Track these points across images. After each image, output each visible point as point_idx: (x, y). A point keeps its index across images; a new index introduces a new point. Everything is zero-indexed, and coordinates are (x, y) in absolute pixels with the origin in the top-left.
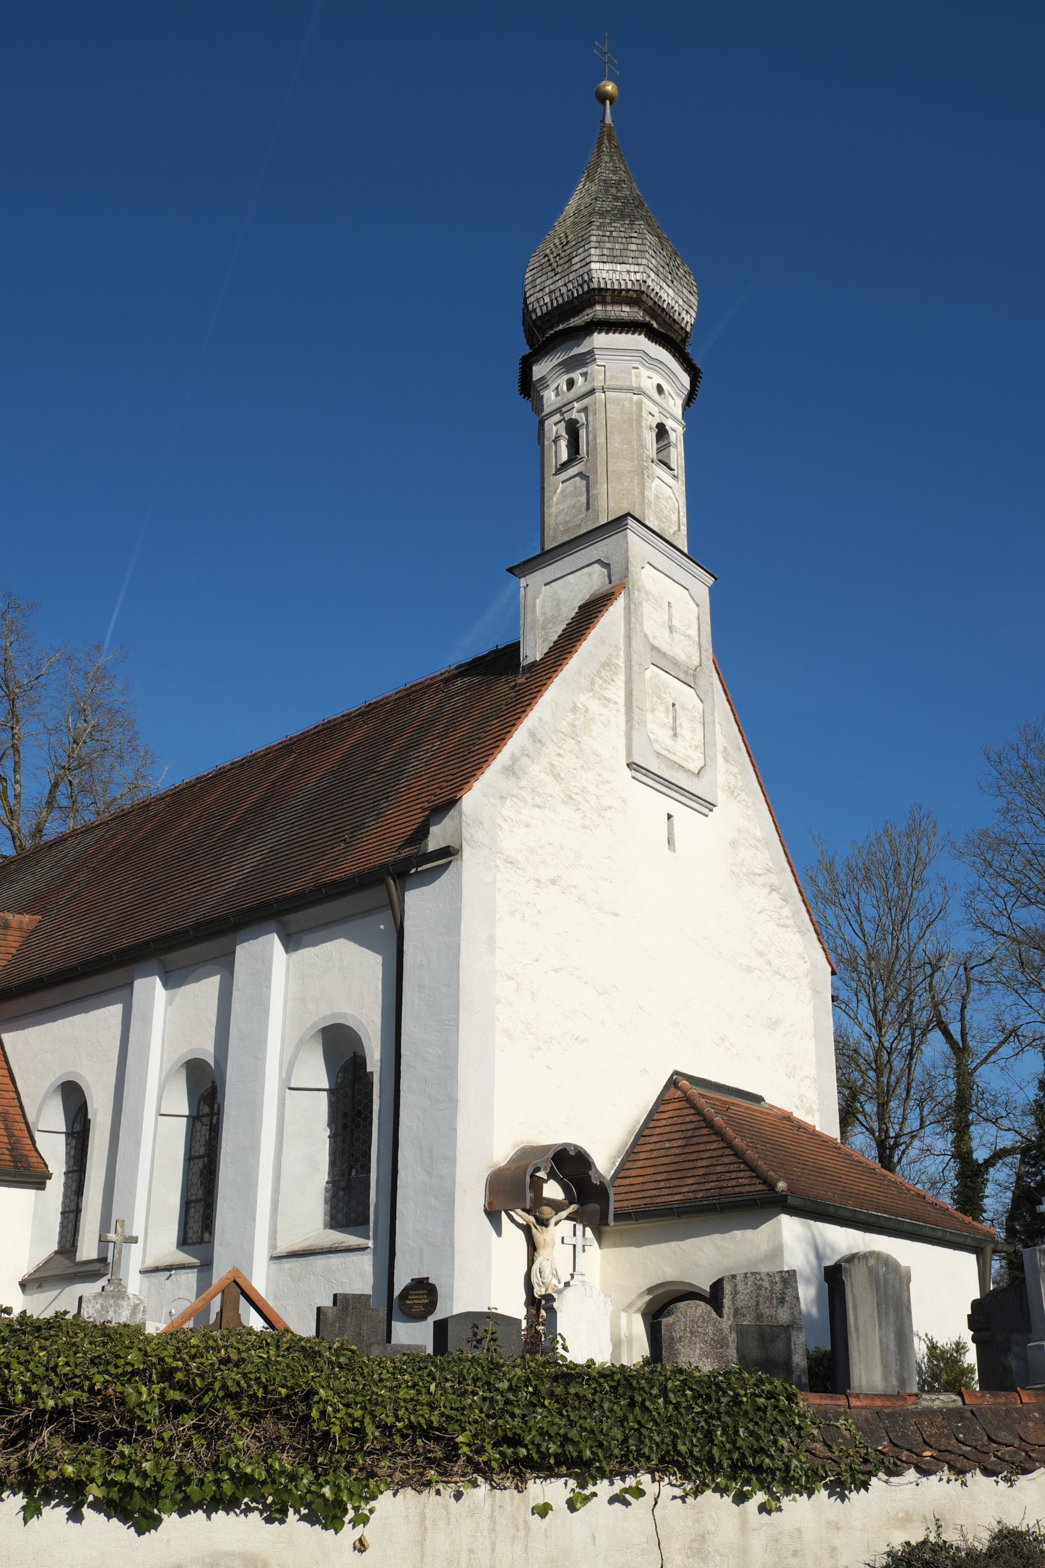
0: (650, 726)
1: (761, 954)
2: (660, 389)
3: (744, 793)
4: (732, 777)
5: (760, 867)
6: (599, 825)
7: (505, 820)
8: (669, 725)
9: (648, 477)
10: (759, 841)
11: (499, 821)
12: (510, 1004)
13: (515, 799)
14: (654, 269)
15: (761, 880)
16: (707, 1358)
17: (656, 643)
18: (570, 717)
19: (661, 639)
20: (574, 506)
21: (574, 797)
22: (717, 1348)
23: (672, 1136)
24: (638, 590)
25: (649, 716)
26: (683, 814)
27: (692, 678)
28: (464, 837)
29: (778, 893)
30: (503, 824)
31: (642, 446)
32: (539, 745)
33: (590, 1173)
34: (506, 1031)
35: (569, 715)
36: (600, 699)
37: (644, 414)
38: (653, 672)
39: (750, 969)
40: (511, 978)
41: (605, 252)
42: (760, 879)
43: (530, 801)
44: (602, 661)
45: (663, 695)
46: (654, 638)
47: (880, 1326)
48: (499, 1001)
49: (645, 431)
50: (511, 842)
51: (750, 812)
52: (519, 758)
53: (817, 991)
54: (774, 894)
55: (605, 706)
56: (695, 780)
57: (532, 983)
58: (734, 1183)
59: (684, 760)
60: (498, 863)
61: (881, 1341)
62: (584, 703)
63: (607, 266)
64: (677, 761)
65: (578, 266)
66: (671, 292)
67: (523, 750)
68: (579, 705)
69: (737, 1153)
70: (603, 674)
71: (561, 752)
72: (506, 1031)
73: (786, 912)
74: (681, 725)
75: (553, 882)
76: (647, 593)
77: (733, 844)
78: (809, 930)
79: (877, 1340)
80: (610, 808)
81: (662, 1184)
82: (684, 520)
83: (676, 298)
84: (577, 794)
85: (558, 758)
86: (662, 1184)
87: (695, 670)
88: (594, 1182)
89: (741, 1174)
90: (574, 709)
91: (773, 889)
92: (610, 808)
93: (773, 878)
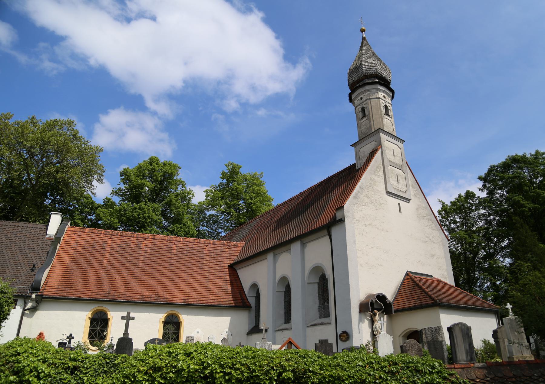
0: (391, 181)
1: (428, 237)
2: (384, 97)
12: (361, 258)
15: (426, 218)
17: (391, 160)
18: (370, 181)
19: (392, 158)
20: (366, 128)
23: (408, 289)
25: (391, 179)
26: (403, 203)
31: (381, 111)
34: (361, 265)
39: (425, 242)
41: (367, 66)
42: (425, 217)
53: (444, 246)
56: (405, 193)
58: (425, 301)
60: (355, 221)
63: (367, 70)
72: (361, 265)
73: (433, 225)
76: (387, 147)
77: (417, 209)
81: (406, 302)
86: (406, 302)
89: (427, 298)
90: (371, 180)
91: (429, 220)
92: (383, 204)
93: (429, 217)
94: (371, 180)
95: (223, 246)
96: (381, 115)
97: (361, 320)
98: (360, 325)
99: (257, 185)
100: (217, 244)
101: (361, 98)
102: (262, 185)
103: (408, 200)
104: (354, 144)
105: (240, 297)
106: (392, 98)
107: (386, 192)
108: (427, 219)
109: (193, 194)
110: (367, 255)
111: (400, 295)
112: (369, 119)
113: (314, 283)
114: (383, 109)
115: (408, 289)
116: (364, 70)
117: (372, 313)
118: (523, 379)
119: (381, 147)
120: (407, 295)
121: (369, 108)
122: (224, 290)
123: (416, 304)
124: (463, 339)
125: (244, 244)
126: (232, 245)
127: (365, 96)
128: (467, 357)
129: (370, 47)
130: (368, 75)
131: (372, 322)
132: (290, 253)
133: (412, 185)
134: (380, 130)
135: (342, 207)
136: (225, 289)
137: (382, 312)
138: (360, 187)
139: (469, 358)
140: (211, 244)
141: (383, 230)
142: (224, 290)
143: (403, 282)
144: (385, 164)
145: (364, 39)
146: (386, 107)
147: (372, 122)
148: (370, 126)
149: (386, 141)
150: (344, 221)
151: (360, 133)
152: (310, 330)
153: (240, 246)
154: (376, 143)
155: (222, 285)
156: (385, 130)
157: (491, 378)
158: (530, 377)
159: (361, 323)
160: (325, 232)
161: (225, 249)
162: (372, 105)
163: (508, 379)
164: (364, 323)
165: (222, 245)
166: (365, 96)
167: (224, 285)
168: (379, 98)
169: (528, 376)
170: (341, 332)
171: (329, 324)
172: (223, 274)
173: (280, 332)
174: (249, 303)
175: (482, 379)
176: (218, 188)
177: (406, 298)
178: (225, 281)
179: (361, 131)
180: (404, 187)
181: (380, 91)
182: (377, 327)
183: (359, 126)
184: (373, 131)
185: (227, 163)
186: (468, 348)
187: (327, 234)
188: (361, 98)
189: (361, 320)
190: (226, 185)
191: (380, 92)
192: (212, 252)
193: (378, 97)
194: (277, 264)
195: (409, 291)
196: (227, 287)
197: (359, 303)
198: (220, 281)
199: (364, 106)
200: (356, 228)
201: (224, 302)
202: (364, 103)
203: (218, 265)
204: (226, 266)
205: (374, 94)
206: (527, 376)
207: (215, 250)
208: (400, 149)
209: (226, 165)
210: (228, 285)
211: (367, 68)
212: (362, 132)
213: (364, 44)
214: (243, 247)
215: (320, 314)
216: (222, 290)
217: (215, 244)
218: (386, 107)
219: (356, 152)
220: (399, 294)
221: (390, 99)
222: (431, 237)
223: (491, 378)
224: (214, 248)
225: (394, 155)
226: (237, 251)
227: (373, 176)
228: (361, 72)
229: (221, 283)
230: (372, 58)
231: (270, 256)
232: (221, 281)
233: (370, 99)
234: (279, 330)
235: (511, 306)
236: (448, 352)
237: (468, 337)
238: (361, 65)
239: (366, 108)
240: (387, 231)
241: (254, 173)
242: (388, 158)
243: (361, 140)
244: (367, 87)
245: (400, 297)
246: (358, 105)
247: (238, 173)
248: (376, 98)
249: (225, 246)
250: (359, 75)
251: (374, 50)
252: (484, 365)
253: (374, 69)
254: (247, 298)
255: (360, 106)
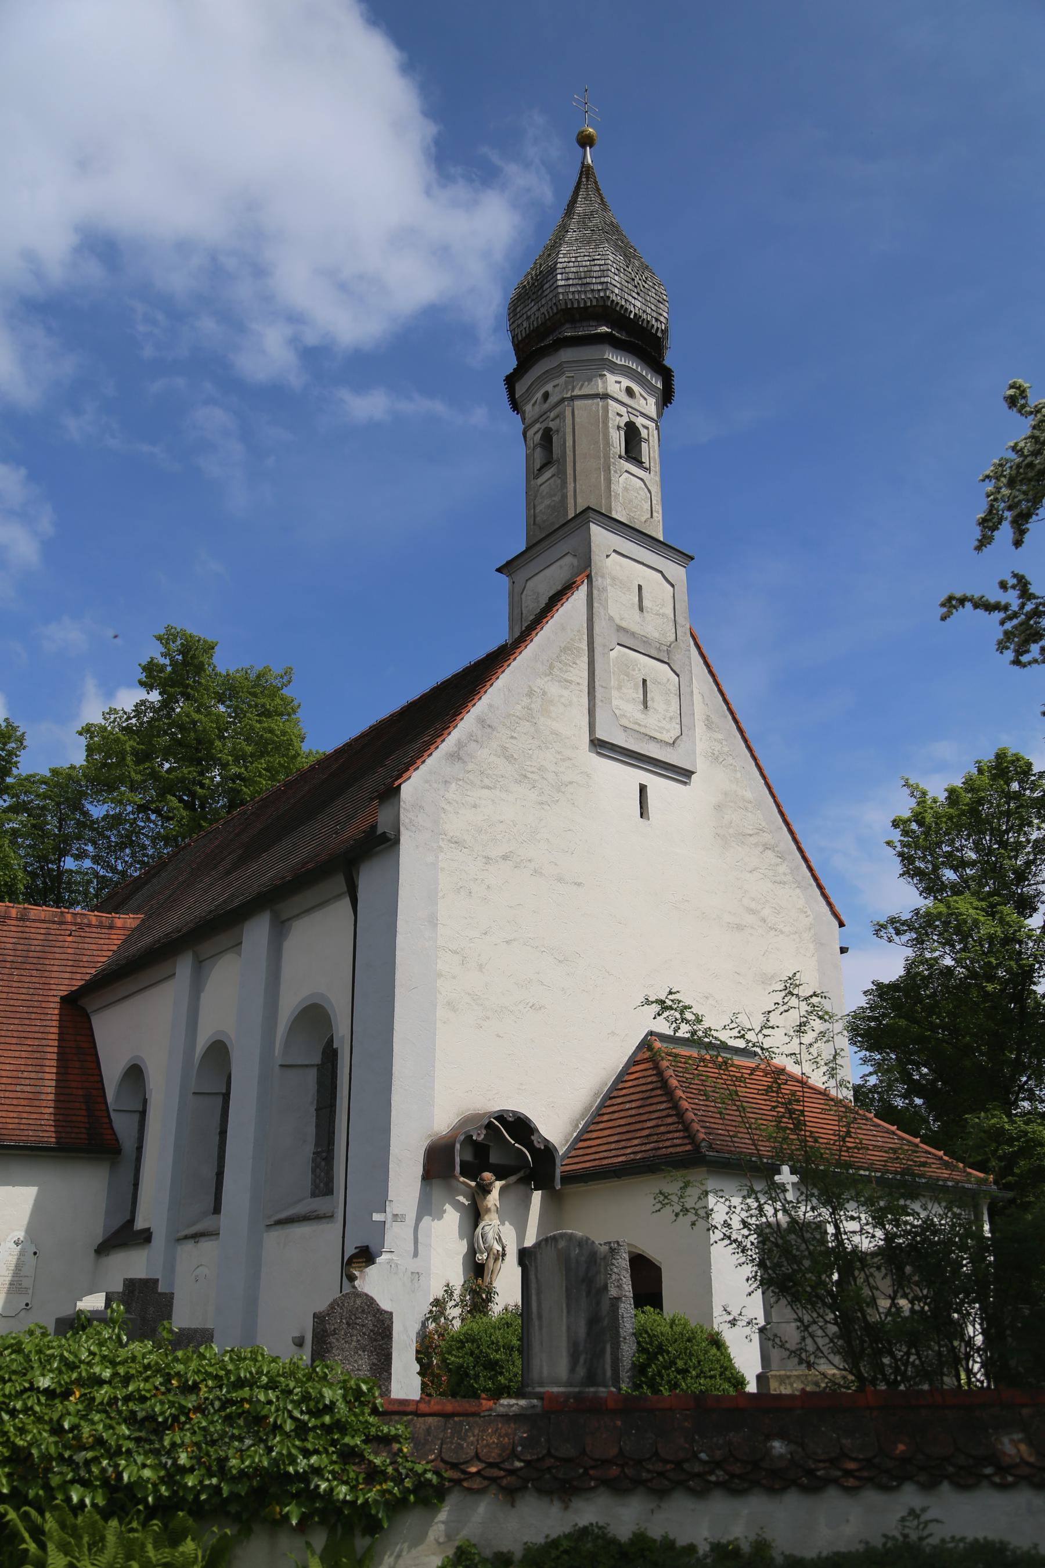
0: (615, 702)
1: (752, 912)
2: (630, 392)
3: (730, 758)
4: (716, 744)
5: (751, 827)
6: (558, 801)
7: (449, 802)
8: (638, 700)
9: (615, 472)
10: (750, 802)
11: (443, 804)
12: (454, 977)
13: (461, 783)
14: (618, 285)
15: (753, 840)
16: (364, 1351)
17: (624, 624)
18: (526, 701)
19: (631, 619)
20: (549, 506)
21: (529, 775)
22: (376, 1340)
23: (633, 1097)
24: (603, 577)
25: (615, 693)
26: (658, 786)
27: (665, 654)
28: (401, 822)
29: (774, 851)
30: (447, 807)
31: (608, 443)
32: (489, 730)
33: (532, 1137)
34: (449, 1003)
35: (524, 699)
36: (560, 681)
37: (610, 415)
38: (619, 651)
39: (739, 928)
40: (455, 952)
41: (571, 276)
42: (751, 839)
43: (479, 783)
44: (563, 646)
45: (631, 672)
46: (622, 619)
47: (568, 1312)
48: (440, 975)
49: (611, 430)
50: (455, 824)
51: (739, 775)
52: (466, 744)
53: (822, 944)
54: (769, 853)
55: (566, 688)
56: (669, 749)
57: (479, 955)
58: (668, 1143)
59: (657, 731)
60: (441, 844)
61: (569, 1329)
62: (542, 686)
63: (572, 289)
64: (648, 733)
65: (548, 291)
66: (638, 304)
67: (471, 737)
68: (535, 689)
69: (680, 1114)
70: (563, 658)
71: (515, 735)
72: (449, 1003)
73: (783, 869)
74: (653, 699)
75: (505, 858)
76: (614, 579)
77: (719, 808)
78: (811, 885)
79: (564, 1328)
80: (571, 783)
81: (613, 1146)
82: (658, 507)
83: (644, 307)
84: (532, 772)
85: (511, 740)
86: (613, 1146)
87: (670, 646)
88: (538, 1146)
89: (677, 1135)
90: (530, 693)
91: (766, 847)
92: (571, 783)
93: (767, 837)
94: (530, 693)
95: (55, 926)
96: (607, 457)
97: (426, 1208)
98: (422, 1225)
99: (266, 714)
100: (34, 921)
101: (546, 396)
102: (289, 715)
103: (683, 774)
104: (509, 563)
105: (84, 1113)
106: (666, 397)
107: (592, 741)
108: (756, 845)
109: (20, 740)
110: (481, 967)
111: (606, 1118)
112: (561, 473)
113: (307, 1066)
114: (617, 440)
115: (633, 1097)
116: (560, 290)
117: (473, 1184)
118: (648, 1471)
119: (589, 577)
120: (622, 1122)
121: (565, 434)
122: (28, 1089)
123: (639, 1156)
124: (568, 1298)
125: (138, 922)
126: (89, 925)
127: (554, 388)
128: (573, 1369)
129: (603, 202)
130: (572, 308)
131: (475, 1215)
132: (240, 955)
133: (708, 718)
134: (591, 514)
135: (391, 793)
136: (32, 1082)
137: (525, 1181)
138: (481, 721)
139: (581, 1372)
140: (10, 918)
141: (560, 879)
142: (28, 1089)
143: (625, 1072)
144: (598, 641)
145: (586, 171)
146: (632, 433)
147: (570, 486)
148: (564, 497)
149: (614, 554)
150: (397, 841)
151: (532, 522)
152: (273, 1239)
153: (119, 928)
154: (575, 562)
155: (23, 1068)
156: (614, 515)
157: (528, 1463)
158: (679, 1464)
159: (427, 1219)
160: (339, 882)
161: (61, 938)
162: (577, 420)
163: (593, 1467)
164: (440, 1218)
165: (54, 922)
166: (557, 389)
167: (30, 1068)
168: (606, 396)
169: (671, 1462)
170: (354, 1251)
171: (329, 1217)
172: (37, 1029)
173: (189, 1246)
174: (114, 1134)
175: (491, 1465)
176: (134, 721)
177: (619, 1130)
178: (38, 1055)
179: (535, 517)
180: (667, 726)
181: (614, 368)
182: (490, 1236)
183: (532, 497)
184: (571, 515)
185: (162, 632)
186: (582, 1331)
187: (345, 889)
188: (546, 396)
189: (426, 1208)
190: (160, 709)
191: (612, 373)
192: (10, 946)
193: (601, 390)
194: (204, 996)
195: (634, 1105)
196: (40, 1075)
197: (424, 1145)
198: (17, 1054)
199: (551, 425)
200: (443, 869)
201: (17, 1132)
202: (552, 415)
203: (23, 997)
204: (51, 999)
205: (590, 380)
206: (666, 1461)
207: (22, 941)
208: (673, 586)
209: (159, 638)
210: (47, 1069)
211: (571, 282)
212: (538, 519)
213: (582, 193)
214: (134, 930)
215: (314, 1182)
216: (18, 1088)
217: (28, 920)
218: (632, 433)
219: (512, 594)
220: (604, 1114)
221: (652, 401)
222: (766, 912)
223: (528, 1463)
224: (20, 935)
225: (641, 609)
226: (105, 947)
227: (540, 683)
228: (551, 295)
229: (23, 1061)
230: (597, 246)
231: (184, 967)
232: (24, 1054)
233: (573, 398)
234: (186, 1237)
235: (795, 1179)
236: (638, 1343)
237: (588, 1293)
238: (553, 270)
239: (558, 431)
240: (579, 884)
241: (259, 668)
242: (611, 619)
243: (533, 548)
244: (566, 355)
245: (601, 1126)
246: (533, 419)
247: (200, 668)
248: (596, 396)
249: (64, 927)
250: (543, 310)
251: (616, 215)
252: (534, 1406)
253: (596, 287)
254: (109, 1116)
255: (538, 426)
